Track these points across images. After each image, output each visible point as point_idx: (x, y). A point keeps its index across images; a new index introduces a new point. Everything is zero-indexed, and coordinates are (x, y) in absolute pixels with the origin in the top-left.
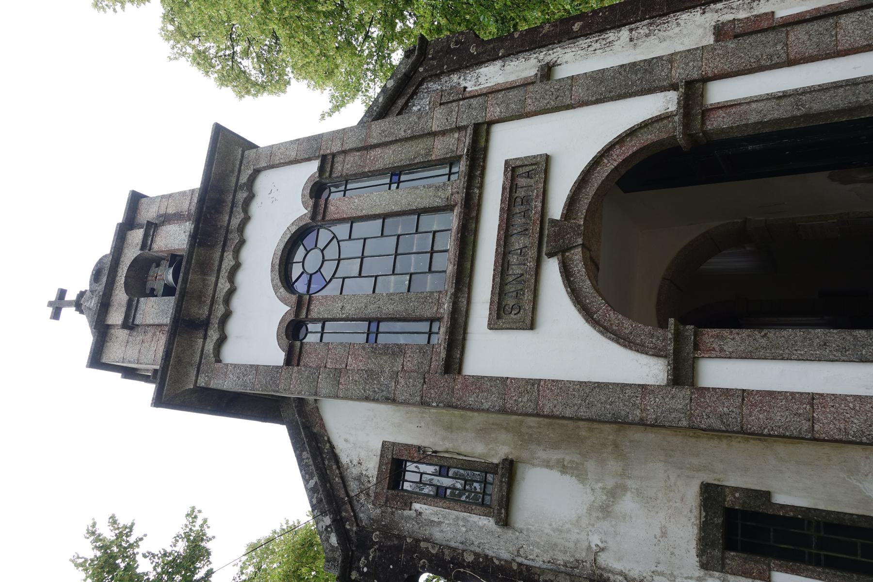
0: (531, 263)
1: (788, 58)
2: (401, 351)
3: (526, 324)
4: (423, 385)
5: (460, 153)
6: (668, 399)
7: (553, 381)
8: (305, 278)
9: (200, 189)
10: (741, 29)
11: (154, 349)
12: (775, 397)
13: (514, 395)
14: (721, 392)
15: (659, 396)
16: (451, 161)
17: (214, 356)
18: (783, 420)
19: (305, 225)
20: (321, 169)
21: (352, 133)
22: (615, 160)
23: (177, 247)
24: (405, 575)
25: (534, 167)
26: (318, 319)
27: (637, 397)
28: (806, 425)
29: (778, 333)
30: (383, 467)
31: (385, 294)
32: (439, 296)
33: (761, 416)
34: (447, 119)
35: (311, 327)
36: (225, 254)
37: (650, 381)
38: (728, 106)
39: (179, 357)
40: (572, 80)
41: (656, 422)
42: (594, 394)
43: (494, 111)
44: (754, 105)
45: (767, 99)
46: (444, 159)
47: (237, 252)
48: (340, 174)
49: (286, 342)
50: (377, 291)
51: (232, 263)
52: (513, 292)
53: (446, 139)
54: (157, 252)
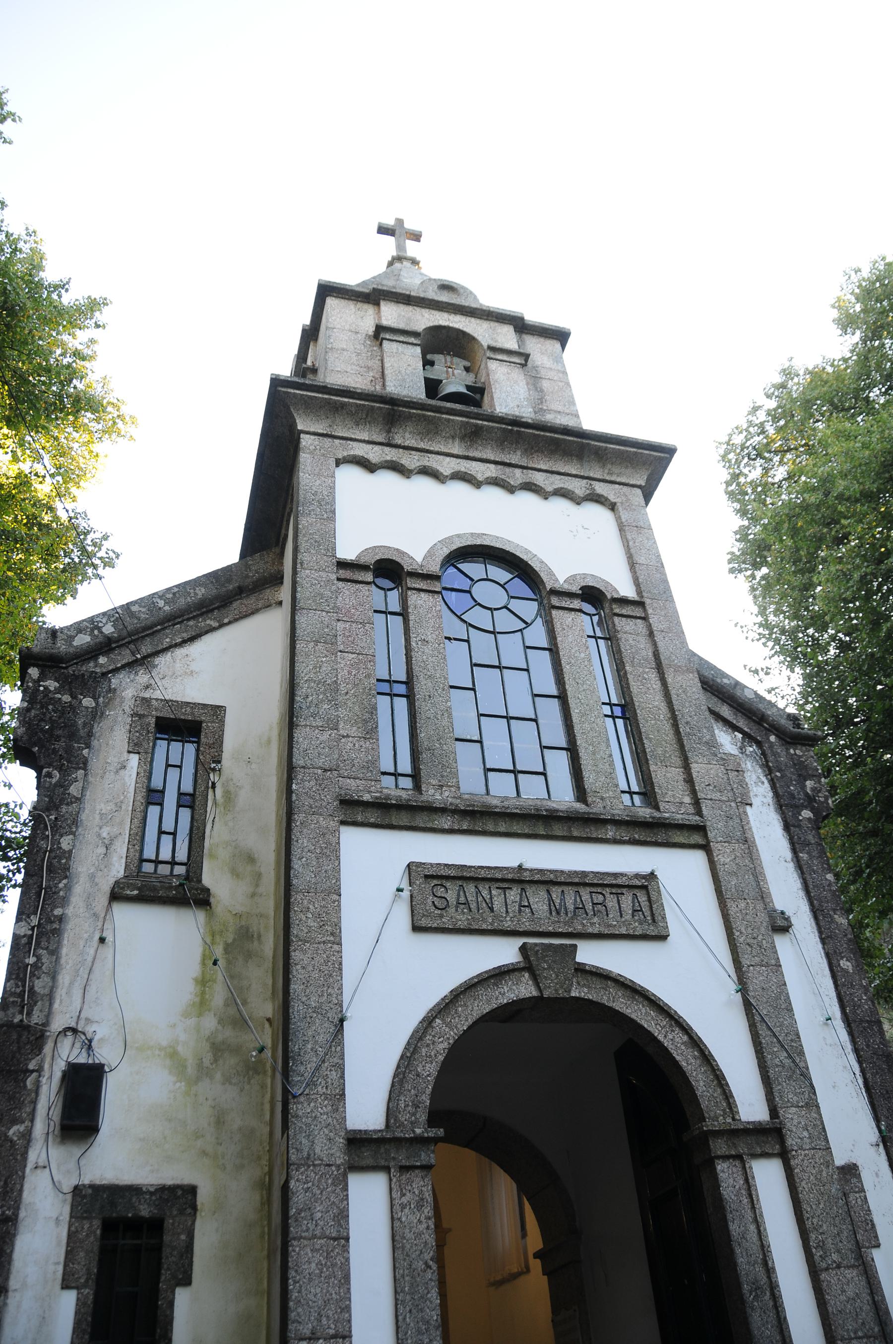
0: (509, 923)
1: (822, 1270)
2: (367, 733)
3: (421, 920)
4: (321, 768)
5: (661, 808)
6: (326, 1131)
7: (341, 964)
8: (465, 584)
9: (582, 428)
10: (854, 1202)
11: (348, 370)
12: (342, 1284)
13: (316, 906)
14: (344, 1207)
15: (330, 1119)
16: (649, 794)
17: (344, 458)
18: (311, 1297)
19: (542, 581)
20: (623, 601)
21: (679, 645)
22: (665, 1036)
23: (495, 396)
24: (37, 748)
25: (649, 918)
26: (407, 607)
27: (327, 1088)
28: (306, 1330)
29: (433, 1283)
30: (188, 709)
31: (449, 704)
32: (452, 786)
33: (313, 1265)
34: (709, 785)
35: (394, 596)
36: (492, 466)
37: (347, 1123)
38: (750, 1191)
39: (342, 408)
40: (775, 965)
41: (293, 1117)
42: (326, 1025)
43: (725, 855)
44: (752, 1227)
45: (762, 1246)
46: (652, 783)
47: (495, 482)
48: (619, 629)
49: (371, 560)
50: (452, 690)
51: (480, 477)
52: (466, 897)
53: (681, 785)
54: (486, 367)
